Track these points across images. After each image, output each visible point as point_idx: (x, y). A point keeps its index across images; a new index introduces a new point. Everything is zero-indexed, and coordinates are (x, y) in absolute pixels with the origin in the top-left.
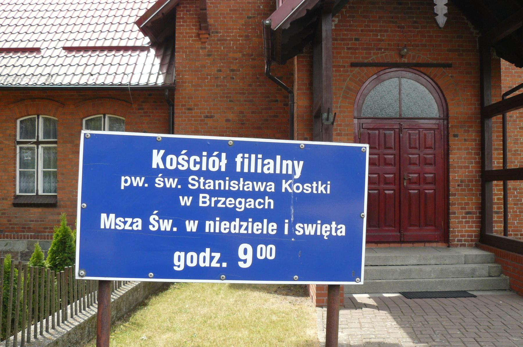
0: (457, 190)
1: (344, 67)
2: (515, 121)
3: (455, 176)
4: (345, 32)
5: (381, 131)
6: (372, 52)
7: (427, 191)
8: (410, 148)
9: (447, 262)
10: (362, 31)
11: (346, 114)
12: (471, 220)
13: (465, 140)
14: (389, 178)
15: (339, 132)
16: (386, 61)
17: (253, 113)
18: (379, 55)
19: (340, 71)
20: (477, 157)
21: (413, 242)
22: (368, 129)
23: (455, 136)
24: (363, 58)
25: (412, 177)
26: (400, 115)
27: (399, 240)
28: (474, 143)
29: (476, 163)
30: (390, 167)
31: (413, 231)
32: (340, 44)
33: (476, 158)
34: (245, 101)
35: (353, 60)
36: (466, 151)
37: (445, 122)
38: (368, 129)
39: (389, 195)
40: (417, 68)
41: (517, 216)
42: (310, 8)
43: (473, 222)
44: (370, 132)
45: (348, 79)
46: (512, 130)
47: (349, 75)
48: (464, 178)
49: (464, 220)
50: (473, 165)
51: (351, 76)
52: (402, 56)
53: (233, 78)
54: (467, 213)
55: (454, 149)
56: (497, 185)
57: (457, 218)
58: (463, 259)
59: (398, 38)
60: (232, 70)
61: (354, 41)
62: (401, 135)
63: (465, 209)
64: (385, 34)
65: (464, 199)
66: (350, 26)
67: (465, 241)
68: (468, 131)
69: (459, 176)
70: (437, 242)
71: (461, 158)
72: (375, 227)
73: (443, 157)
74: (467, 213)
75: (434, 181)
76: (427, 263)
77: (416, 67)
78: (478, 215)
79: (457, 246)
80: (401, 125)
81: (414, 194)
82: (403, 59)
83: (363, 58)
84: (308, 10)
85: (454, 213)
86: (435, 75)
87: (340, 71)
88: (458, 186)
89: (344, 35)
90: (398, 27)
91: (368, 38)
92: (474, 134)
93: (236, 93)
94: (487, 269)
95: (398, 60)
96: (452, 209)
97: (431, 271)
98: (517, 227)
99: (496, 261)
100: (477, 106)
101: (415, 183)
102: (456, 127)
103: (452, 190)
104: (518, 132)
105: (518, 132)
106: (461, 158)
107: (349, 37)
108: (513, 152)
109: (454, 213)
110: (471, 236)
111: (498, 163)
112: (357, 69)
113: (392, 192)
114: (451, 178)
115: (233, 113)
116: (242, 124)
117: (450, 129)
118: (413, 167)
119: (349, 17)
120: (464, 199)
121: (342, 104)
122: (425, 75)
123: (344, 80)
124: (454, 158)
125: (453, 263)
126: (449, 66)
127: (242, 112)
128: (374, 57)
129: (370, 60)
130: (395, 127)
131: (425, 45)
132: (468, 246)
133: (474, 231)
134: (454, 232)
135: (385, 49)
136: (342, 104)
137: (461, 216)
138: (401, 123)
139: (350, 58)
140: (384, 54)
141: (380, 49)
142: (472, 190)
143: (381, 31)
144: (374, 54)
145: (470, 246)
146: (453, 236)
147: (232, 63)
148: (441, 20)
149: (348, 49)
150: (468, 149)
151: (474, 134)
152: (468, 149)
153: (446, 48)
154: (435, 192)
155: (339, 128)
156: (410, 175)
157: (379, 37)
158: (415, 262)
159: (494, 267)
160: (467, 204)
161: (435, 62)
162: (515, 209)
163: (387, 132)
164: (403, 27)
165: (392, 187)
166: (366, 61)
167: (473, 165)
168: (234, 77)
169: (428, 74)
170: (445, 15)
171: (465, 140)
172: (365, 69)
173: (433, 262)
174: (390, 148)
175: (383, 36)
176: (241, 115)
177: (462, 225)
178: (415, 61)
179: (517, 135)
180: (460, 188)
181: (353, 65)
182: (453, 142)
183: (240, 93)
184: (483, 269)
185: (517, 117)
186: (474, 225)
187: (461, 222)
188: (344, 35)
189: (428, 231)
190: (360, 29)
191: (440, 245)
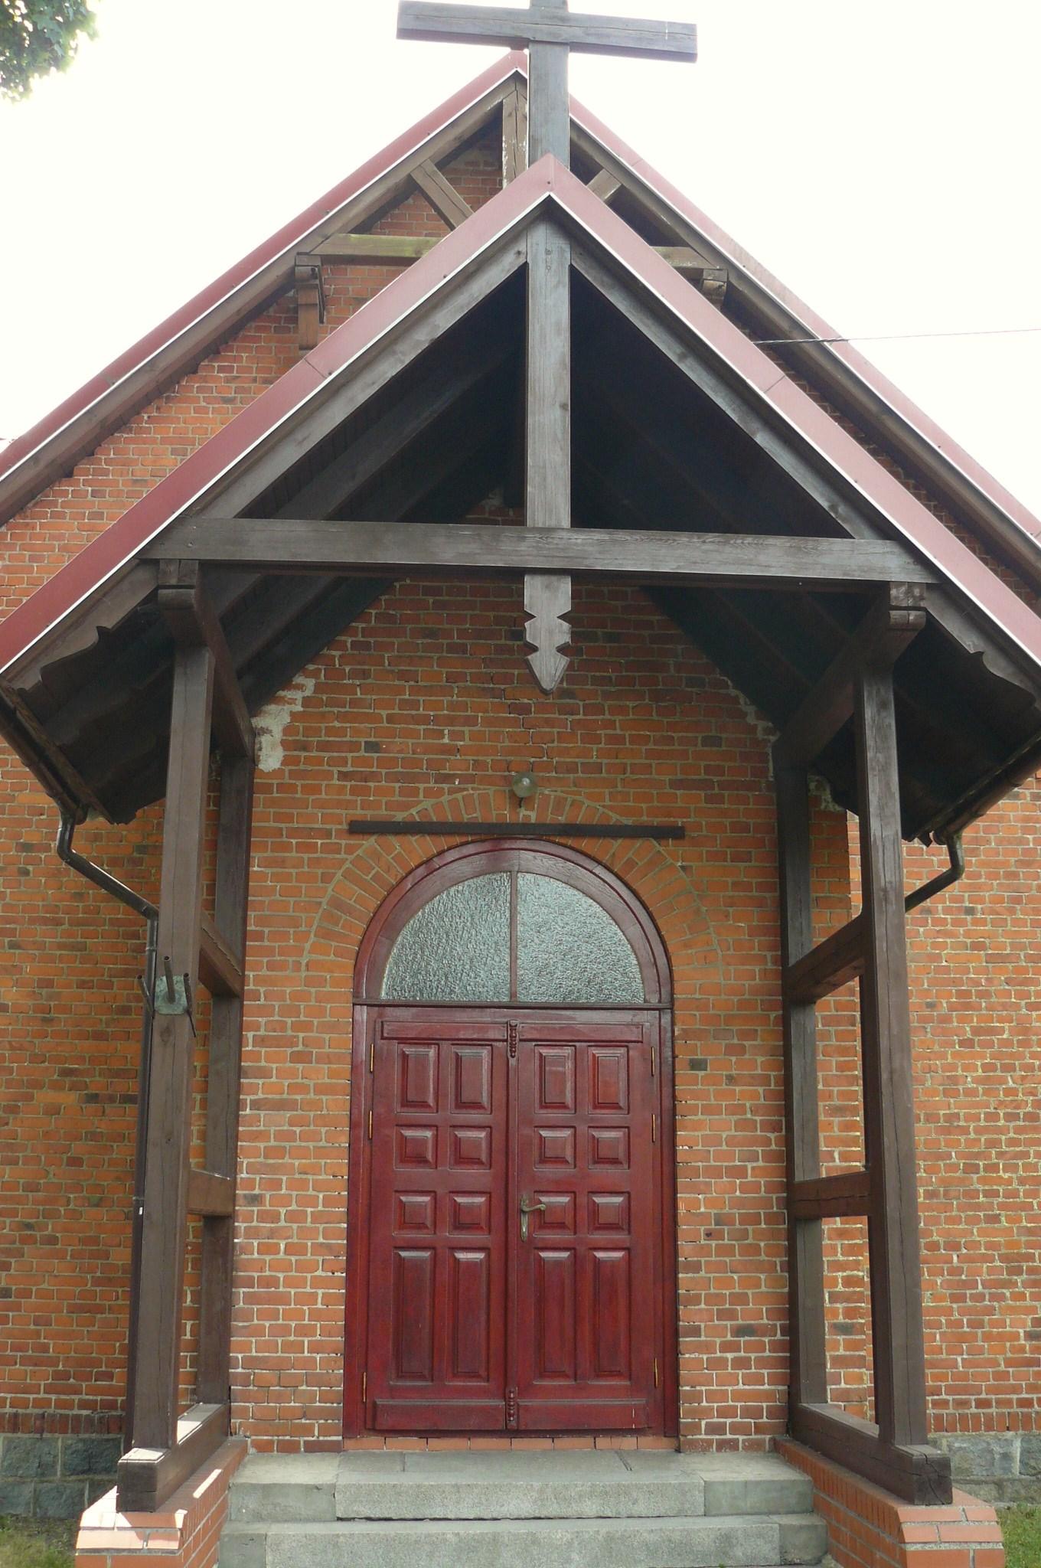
0: (705, 1251)
1: (327, 834)
2: (946, 1019)
3: (699, 1202)
4: (337, 724)
5: (445, 1045)
6: (421, 786)
7: (600, 1255)
8: (545, 1105)
9: (640, 1509)
10: (391, 719)
11: (328, 989)
12: (753, 1356)
13: (731, 1079)
14: (470, 1208)
15: (300, 1048)
16: (466, 818)
17: (82, 985)
18: (445, 798)
19: (312, 848)
20: (772, 1136)
21: (553, 1433)
22: (403, 1040)
23: (697, 1065)
24: (389, 806)
25: (549, 1206)
26: (513, 995)
27: (501, 1426)
28: (761, 1089)
29: (769, 1156)
30: (474, 1171)
31: (551, 1396)
32: (319, 761)
33: (768, 1142)
34: (61, 946)
35: (359, 813)
36: (734, 1118)
37: (666, 1019)
38: (403, 1040)
39: (470, 1264)
40: (570, 842)
41: (963, 1338)
42: (109, 623)
43: (762, 1363)
44: (409, 1050)
45: (339, 876)
46: (936, 1048)
47: (344, 861)
48: (727, 1210)
49: (730, 1356)
50: (761, 1163)
51: (348, 865)
52: (519, 802)
53: (26, 873)
54: (740, 1331)
55: (694, 1110)
56: (842, 1234)
57: (708, 1347)
58: (700, 1498)
59: (507, 743)
60: (26, 847)
61: (362, 753)
62: (512, 1062)
63: (730, 1315)
64: (466, 729)
65: (729, 1282)
66: (354, 703)
67: (735, 1428)
68: (742, 1050)
69: (709, 1203)
70: (638, 1432)
71: (716, 1141)
72: (422, 1377)
73: (656, 1135)
74: (740, 1331)
75: (626, 1220)
76: (569, 1512)
77: (565, 836)
78: (779, 1336)
79: (704, 1447)
80: (513, 1028)
81: (558, 1263)
82: (523, 812)
83: (389, 806)
84: (101, 630)
85: (696, 1331)
86: (630, 864)
87: (312, 848)
88: (709, 1235)
89: (330, 731)
90: (512, 708)
91: (410, 741)
92: (760, 1059)
93: (32, 921)
94: (777, 1536)
95: (507, 815)
96: (687, 1315)
97: (570, 1544)
98: (964, 1377)
99: (815, 1507)
100: (770, 966)
101: (561, 1226)
102: (699, 1035)
103: (686, 1250)
104: (955, 1055)
105: (955, 1055)
106: (716, 1141)
107: (348, 739)
108: (942, 1123)
109: (696, 1331)
110: (756, 1413)
111: (844, 1157)
112: (371, 842)
113: (481, 1256)
114: (682, 1210)
115: (17, 984)
116: (45, 1021)
117: (679, 1042)
118: (549, 1171)
119: (354, 674)
120: (729, 1282)
121: (314, 956)
122: (599, 863)
123: (327, 878)
124: (693, 1139)
125: (662, 1512)
126: (676, 833)
127: (49, 984)
128: (427, 804)
129: (414, 814)
130: (491, 1035)
131: (598, 768)
132: (745, 1448)
133: (767, 1396)
134: (696, 1397)
135: (467, 779)
136: (314, 956)
137: (718, 1341)
138: (513, 1023)
139: (348, 805)
140: (459, 796)
141: (448, 778)
142: (756, 1250)
143: (451, 721)
144: (428, 793)
145: (753, 1447)
146: (693, 1413)
147: (28, 823)
148: (549, 666)
149: (344, 776)
150: (741, 1109)
151: (760, 1059)
152: (741, 1109)
153: (667, 778)
154: (629, 1260)
155: (301, 1035)
156: (544, 1199)
157: (446, 740)
158: (527, 1508)
159: (801, 1527)
160: (742, 1299)
161: (628, 821)
162: (956, 1316)
163: (466, 1052)
164: (525, 710)
165: (566, 1236)
166: (400, 816)
167: (761, 1163)
168: (30, 868)
169: (606, 859)
170: (562, 650)
171: (731, 1079)
172: (393, 840)
173: (590, 1507)
174: (476, 1106)
175: (459, 736)
176: (44, 991)
177: (724, 1371)
178: (562, 819)
179: (954, 1068)
180: (714, 1243)
181: (357, 828)
182: (691, 1088)
183: (45, 921)
184: (760, 1535)
185: (952, 1008)
186: (765, 1372)
187: (721, 1363)
188: (330, 731)
189: (610, 1395)
190: (384, 713)
191: (647, 1441)
